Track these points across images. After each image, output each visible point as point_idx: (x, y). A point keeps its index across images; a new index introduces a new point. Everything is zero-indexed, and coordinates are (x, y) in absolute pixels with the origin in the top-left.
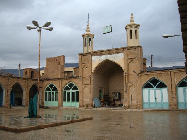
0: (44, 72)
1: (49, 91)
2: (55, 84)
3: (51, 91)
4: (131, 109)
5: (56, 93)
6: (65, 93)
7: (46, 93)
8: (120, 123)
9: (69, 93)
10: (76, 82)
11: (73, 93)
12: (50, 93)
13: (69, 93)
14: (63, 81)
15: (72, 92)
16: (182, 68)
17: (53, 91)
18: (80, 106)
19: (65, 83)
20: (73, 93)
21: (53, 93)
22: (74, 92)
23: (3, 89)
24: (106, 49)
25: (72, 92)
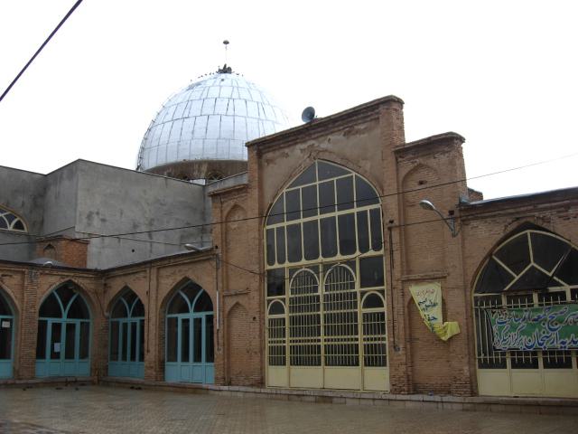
0: (536, 290)
1: (57, 320)
2: (140, 286)
3: (64, 320)
4: (461, 217)
5: (85, 327)
6: (173, 322)
7: (42, 326)
8: (575, 201)
9: (125, 325)
10: (206, 278)
11: (134, 325)
12: (57, 327)
13: (125, 325)
14: (164, 272)
15: (67, 325)
16: (375, 398)
17: (71, 321)
18: (396, 389)
19: (169, 281)
20: (198, 321)
21: (198, 321)
22: (135, 323)
23: (86, 308)
24: (282, 130)
25: (53, 324)
